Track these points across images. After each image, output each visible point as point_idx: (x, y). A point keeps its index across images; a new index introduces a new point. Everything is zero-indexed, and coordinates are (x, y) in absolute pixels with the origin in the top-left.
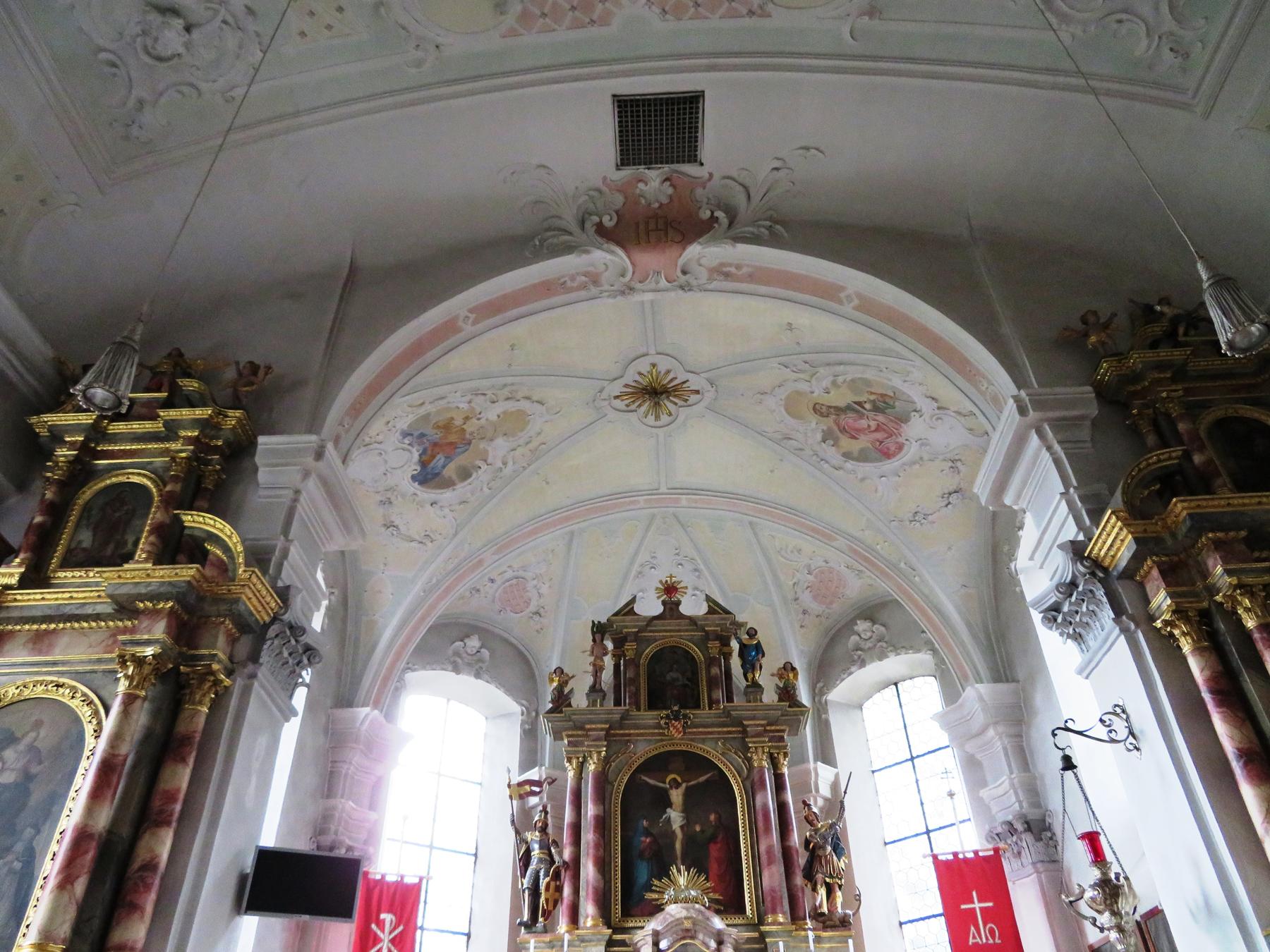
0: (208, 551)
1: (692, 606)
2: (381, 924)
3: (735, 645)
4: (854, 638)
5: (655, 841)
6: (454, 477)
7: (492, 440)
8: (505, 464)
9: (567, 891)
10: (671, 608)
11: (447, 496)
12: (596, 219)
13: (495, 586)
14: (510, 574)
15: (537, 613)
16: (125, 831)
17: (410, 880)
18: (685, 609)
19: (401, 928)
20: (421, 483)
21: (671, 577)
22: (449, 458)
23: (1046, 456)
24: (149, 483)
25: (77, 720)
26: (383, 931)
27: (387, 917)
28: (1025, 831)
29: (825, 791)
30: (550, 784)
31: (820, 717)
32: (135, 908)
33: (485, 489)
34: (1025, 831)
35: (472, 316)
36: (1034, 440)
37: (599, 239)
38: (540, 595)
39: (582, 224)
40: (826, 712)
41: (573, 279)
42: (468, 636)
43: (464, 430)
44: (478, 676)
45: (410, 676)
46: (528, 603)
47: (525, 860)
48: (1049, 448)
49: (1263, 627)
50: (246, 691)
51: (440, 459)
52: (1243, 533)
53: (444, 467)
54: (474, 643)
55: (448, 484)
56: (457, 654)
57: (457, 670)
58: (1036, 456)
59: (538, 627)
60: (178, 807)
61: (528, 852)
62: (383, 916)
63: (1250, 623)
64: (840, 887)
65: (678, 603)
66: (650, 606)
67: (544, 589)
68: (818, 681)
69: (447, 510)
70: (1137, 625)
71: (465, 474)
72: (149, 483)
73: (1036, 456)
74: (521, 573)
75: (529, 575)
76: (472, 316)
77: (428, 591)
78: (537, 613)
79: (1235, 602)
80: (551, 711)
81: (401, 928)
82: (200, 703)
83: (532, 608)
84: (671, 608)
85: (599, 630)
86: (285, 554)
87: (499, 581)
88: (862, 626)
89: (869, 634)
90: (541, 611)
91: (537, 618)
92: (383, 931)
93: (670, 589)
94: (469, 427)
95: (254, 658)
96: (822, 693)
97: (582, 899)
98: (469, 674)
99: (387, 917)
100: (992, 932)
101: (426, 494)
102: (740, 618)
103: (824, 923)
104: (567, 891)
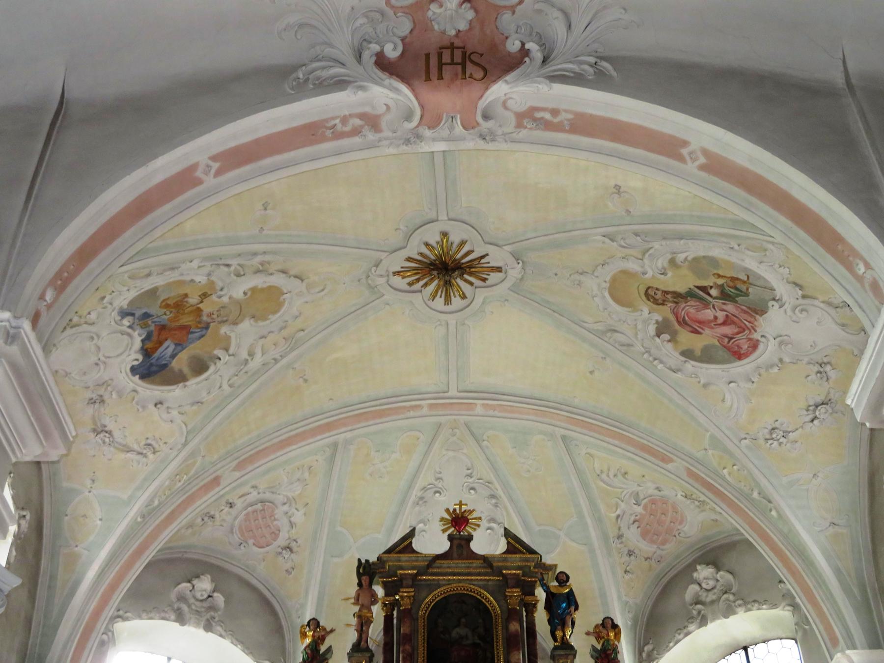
1: (487, 543)
4: (693, 588)
6: (186, 370)
7: (235, 323)
8: (251, 354)
10: (460, 544)
11: (175, 393)
12: (376, 48)
13: (234, 512)
14: (254, 496)
15: (288, 548)
18: (479, 546)
20: (142, 377)
21: (461, 504)
22: (180, 345)
33: (225, 386)
35: (216, 166)
37: (379, 73)
38: (292, 525)
39: (359, 57)
41: (344, 120)
42: (198, 577)
43: (199, 311)
44: (208, 627)
45: (120, 627)
46: (275, 534)
51: (169, 347)
53: (173, 356)
54: (204, 585)
55: (178, 378)
56: (182, 598)
57: (181, 619)
59: (288, 565)
65: (470, 538)
66: (433, 542)
67: (298, 517)
69: (175, 413)
71: (200, 367)
74: (268, 496)
75: (280, 499)
76: (216, 166)
77: (146, 515)
78: (288, 548)
83: (282, 541)
84: (460, 544)
85: (367, 572)
87: (239, 504)
88: (704, 572)
89: (712, 583)
90: (293, 545)
91: (286, 554)
93: (459, 521)
94: (206, 308)
98: (197, 625)
101: (149, 391)
102: (548, 560)
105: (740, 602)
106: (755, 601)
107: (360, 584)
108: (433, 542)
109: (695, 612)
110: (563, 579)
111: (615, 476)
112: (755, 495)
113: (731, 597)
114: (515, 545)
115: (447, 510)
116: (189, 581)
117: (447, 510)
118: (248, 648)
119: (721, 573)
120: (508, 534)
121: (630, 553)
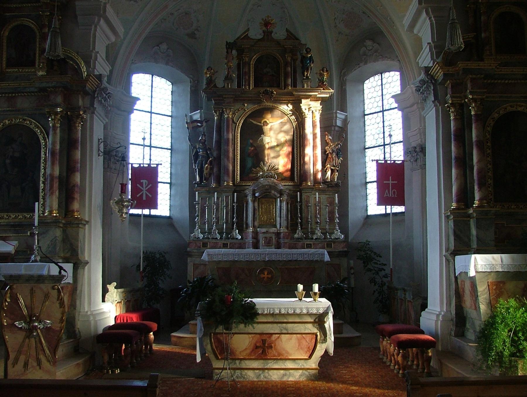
0: (68, 62)
1: (279, 34)
2: (142, 184)
3: (299, 57)
4: (363, 49)
5: (255, 149)
9: (215, 170)
10: (268, 34)
15: (197, 30)
16: (65, 174)
17: (159, 207)
18: (274, 36)
19: (151, 185)
21: (268, 17)
23: (428, 21)
24: (35, 28)
25: (35, 133)
26: (143, 187)
27: (144, 181)
28: (421, 151)
29: (339, 123)
30: (206, 122)
31: (342, 87)
32: (73, 199)
34: (421, 151)
36: (424, 15)
40: (345, 85)
42: (161, 43)
44: (167, 64)
47: (196, 156)
48: (430, 18)
49: (476, 115)
50: (92, 119)
52: (482, 76)
54: (164, 47)
58: (425, 20)
60: (79, 165)
61: (197, 153)
62: (142, 181)
63: (473, 113)
64: (337, 171)
65: (271, 32)
66: (256, 33)
68: (343, 69)
70: (440, 105)
72: (35, 28)
73: (425, 20)
79: (471, 104)
80: (206, 89)
81: (151, 185)
82: (78, 126)
84: (268, 34)
85: (230, 46)
86: (96, 59)
88: (369, 43)
89: (371, 48)
90: (199, 29)
92: (143, 187)
93: (267, 24)
95: (92, 104)
96: (345, 75)
97: (222, 173)
99: (144, 181)
100: (394, 192)
102: (303, 42)
103: (328, 185)
104: (215, 170)
105: (381, 57)
106: (386, 57)
107: (227, 52)
108: (256, 33)
109: (363, 59)
110: (308, 51)
111: (335, 2)
112: (388, 19)
113: (378, 54)
114: (291, 36)
115: (263, 19)
116: (158, 46)
117: (263, 19)
118: (283, 389)
119: (375, 44)
120: (287, 30)
121: (339, 33)
